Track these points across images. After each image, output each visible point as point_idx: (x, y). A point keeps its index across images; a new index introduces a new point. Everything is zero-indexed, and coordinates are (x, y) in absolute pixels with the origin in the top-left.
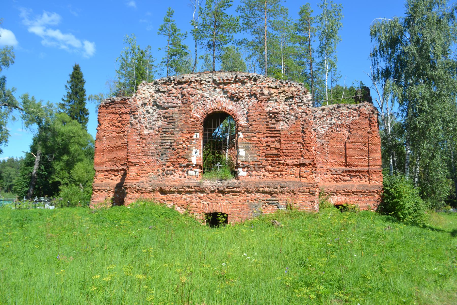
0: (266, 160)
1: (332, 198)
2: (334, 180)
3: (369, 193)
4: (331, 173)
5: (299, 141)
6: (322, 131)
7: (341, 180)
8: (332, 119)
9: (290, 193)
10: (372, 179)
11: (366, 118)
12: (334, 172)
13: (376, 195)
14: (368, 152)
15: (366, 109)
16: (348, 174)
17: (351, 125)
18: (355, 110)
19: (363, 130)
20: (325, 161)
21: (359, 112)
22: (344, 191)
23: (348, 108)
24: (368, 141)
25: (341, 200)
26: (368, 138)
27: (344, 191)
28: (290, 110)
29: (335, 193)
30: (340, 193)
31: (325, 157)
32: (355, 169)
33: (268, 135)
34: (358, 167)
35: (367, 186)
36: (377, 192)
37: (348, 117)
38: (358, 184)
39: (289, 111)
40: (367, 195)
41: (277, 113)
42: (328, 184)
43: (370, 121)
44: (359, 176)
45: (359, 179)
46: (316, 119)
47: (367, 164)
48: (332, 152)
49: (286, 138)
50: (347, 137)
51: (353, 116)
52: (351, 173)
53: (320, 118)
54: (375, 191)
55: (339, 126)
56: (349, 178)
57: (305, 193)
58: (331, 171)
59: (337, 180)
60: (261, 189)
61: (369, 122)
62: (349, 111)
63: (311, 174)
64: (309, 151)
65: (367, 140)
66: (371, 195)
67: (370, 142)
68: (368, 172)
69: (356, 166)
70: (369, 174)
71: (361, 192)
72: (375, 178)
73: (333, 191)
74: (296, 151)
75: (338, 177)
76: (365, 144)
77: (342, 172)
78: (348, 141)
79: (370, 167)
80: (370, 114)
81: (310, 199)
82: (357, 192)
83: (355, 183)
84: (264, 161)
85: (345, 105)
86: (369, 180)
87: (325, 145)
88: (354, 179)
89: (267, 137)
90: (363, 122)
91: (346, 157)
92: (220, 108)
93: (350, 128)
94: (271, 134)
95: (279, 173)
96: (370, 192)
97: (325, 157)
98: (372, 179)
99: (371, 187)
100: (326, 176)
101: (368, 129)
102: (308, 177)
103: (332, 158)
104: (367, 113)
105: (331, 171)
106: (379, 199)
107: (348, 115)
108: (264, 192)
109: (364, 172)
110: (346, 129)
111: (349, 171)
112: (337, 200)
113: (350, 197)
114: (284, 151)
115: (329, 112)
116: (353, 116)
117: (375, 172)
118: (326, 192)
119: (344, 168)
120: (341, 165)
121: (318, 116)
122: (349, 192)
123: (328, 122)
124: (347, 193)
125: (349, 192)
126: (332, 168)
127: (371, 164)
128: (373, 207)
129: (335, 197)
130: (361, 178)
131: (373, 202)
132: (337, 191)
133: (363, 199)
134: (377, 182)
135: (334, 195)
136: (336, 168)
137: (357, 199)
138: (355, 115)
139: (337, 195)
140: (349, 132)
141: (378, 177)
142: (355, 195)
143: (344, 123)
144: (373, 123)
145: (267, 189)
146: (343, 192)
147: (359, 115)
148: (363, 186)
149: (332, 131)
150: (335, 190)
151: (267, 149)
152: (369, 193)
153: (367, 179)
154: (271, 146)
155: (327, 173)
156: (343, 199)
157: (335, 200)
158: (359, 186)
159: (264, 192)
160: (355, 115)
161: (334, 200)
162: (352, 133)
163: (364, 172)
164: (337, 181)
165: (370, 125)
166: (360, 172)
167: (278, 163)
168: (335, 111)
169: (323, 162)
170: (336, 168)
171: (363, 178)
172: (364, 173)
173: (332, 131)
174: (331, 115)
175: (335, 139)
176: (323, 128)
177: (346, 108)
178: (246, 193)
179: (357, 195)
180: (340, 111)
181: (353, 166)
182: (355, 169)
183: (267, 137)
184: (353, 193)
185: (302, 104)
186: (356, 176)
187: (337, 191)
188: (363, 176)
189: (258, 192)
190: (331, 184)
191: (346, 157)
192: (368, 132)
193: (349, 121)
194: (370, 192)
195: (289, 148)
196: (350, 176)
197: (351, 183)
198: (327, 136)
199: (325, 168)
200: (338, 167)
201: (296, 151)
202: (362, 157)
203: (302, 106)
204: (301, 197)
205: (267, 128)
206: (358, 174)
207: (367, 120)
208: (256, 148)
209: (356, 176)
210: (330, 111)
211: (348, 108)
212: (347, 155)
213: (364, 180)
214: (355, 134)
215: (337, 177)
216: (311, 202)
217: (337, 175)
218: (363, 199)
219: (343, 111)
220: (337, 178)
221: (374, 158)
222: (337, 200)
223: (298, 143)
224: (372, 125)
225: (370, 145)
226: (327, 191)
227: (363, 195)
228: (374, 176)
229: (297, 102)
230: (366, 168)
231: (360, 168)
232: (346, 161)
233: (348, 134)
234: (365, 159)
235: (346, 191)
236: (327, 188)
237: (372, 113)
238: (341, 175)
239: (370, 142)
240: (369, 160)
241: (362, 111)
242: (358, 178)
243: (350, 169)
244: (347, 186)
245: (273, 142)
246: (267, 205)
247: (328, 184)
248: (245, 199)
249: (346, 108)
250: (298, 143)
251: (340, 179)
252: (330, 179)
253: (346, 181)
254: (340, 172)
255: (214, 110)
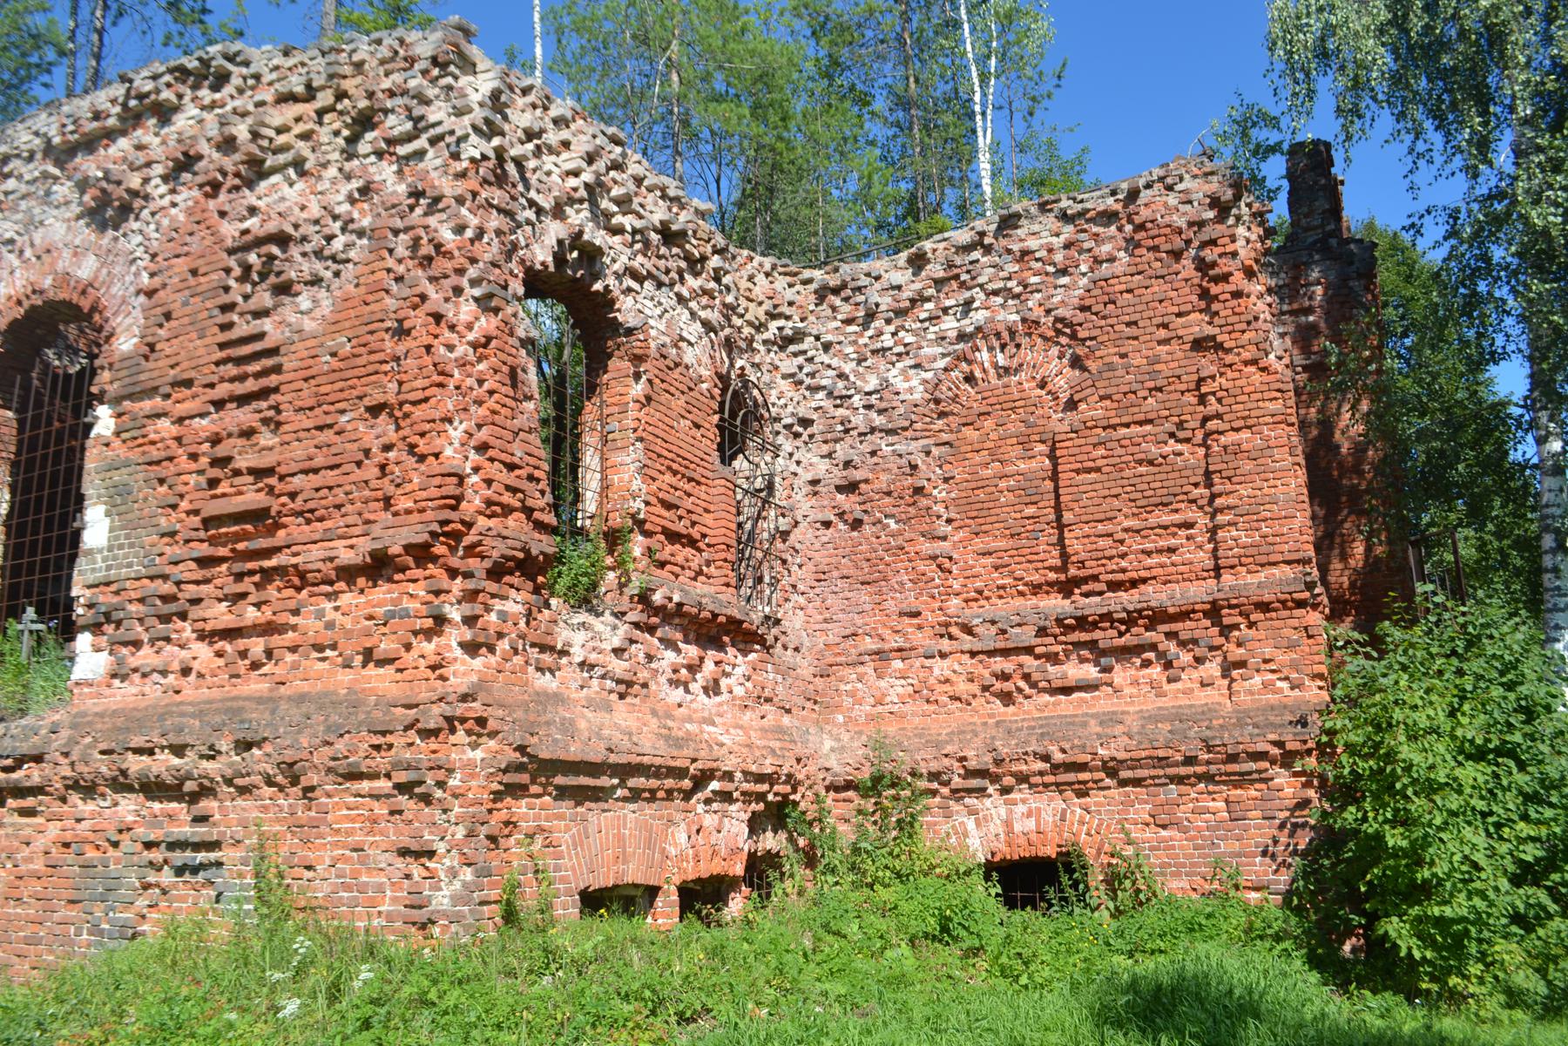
0: (204, 562)
1: (972, 812)
2: (985, 688)
3: (1222, 766)
4: (967, 642)
5: (376, 397)
6: (911, 386)
7: (1034, 685)
8: (968, 305)
9: (281, 789)
10: (1242, 664)
11: (1177, 255)
12: (988, 637)
13: (1281, 777)
14: (1208, 474)
15: (1172, 200)
16: (1078, 645)
17: (1080, 317)
18: (1109, 217)
19: (1163, 333)
20: (930, 569)
21: (1129, 228)
22: (1046, 758)
23: (1065, 217)
24: (1202, 400)
25: (1031, 824)
26: (1200, 381)
27: (1046, 758)
28: (352, 201)
29: (985, 777)
30: (1022, 778)
31: (927, 547)
32: (1128, 599)
33: (223, 390)
34: (1148, 589)
35: (1208, 712)
36: (1287, 759)
37: (1064, 272)
38: (1152, 704)
39: (344, 208)
40: (1208, 778)
41: (282, 240)
42: (946, 721)
43: (1202, 266)
44: (1153, 647)
45: (1156, 671)
46: (878, 323)
47: (1203, 558)
48: (975, 512)
49: (308, 390)
50: (1064, 397)
51: (1098, 261)
52: (1097, 634)
53: (901, 313)
54: (1262, 747)
55: (1007, 339)
56: (1091, 672)
57: (365, 785)
58: (968, 630)
59: (1008, 686)
60: (135, 764)
61: (1196, 277)
62: (1068, 231)
63: (428, 634)
64: (422, 458)
65: (1190, 398)
66: (1242, 780)
67: (1213, 406)
68: (1214, 611)
69: (1134, 583)
70: (1226, 631)
71: (1162, 761)
72: (1268, 652)
73: (972, 764)
74: (359, 475)
75: (1010, 666)
76: (1180, 425)
77: (1042, 632)
78: (1059, 422)
79: (1227, 578)
80: (1201, 224)
81: (396, 834)
82: (1136, 763)
83: (1133, 702)
84: (189, 571)
85: (1043, 207)
86: (1228, 668)
87: (929, 471)
88: (1122, 674)
89: (219, 404)
90: (1158, 287)
91: (1061, 527)
92: (48, 282)
93: (1073, 336)
94: (242, 378)
95: (257, 646)
96: (1233, 758)
97: (927, 547)
98: (1242, 664)
99: (1241, 724)
100: (940, 667)
101: (1197, 325)
102: (409, 658)
103: (979, 544)
104: (1181, 222)
105: (968, 630)
106: (1304, 804)
107: (1059, 257)
108: (153, 789)
109: (1184, 615)
110: (1055, 351)
111: (1082, 623)
112: (1008, 824)
113: (1096, 798)
114: (297, 481)
115: (950, 265)
116: (1098, 261)
117: (1264, 607)
118: (934, 776)
119: (1056, 604)
120: (1036, 589)
121: (886, 302)
122: (1083, 767)
123: (950, 324)
124: (1069, 775)
125: (1083, 767)
126: (975, 614)
127: (1228, 555)
128: (1260, 868)
129: (993, 805)
130: (1168, 665)
131: (1259, 832)
132: (998, 762)
133: (1181, 813)
134: (1282, 678)
135: (981, 792)
136: (1002, 608)
137: (1142, 811)
138: (1106, 248)
139: (1006, 791)
140: (1076, 362)
141: (1291, 647)
142: (1123, 783)
143: (1038, 313)
144: (1225, 278)
145: (163, 764)
146: (1040, 765)
147: (1132, 245)
148: (1178, 716)
149: (970, 379)
150: (988, 758)
151: (213, 483)
152: (1222, 766)
153: (1213, 668)
154: (241, 463)
155: (945, 645)
156: (1048, 818)
157: (996, 827)
158: (1155, 718)
159: (153, 789)
160: (1106, 248)
161: (988, 827)
162: (1092, 365)
163: (1184, 615)
164: (1007, 698)
165: (1204, 294)
166: (1157, 617)
167: (262, 570)
168: (988, 250)
169: (919, 579)
170: (1002, 608)
171: (1186, 657)
172: (1184, 628)
173: (970, 379)
174: (963, 285)
175: (989, 423)
176: (917, 366)
177: (1050, 221)
178: (74, 798)
179: (1137, 782)
180: (1015, 247)
181: (1114, 586)
182: (1128, 599)
183: (219, 404)
184: (1111, 769)
185: (421, 143)
186: (1138, 649)
187: (998, 762)
188: (1183, 644)
189: (121, 783)
190: (967, 716)
191: (1061, 527)
192: (1199, 345)
193: (1066, 296)
194: (1233, 758)
195: (319, 461)
196: (1097, 652)
197: (1101, 702)
198: (942, 415)
199: (929, 617)
200: (1019, 602)
201: (359, 475)
202: (1166, 519)
203: (420, 154)
204: (343, 807)
205: (222, 346)
206: (1117, 631)
207: (1187, 267)
208: (163, 489)
209: (1138, 649)
210: (958, 261)
211: (1065, 217)
212: (1068, 517)
213: (1190, 678)
214: (1111, 367)
215: (1006, 665)
216: (404, 852)
217: (1005, 652)
218: (1181, 813)
219: (1032, 244)
220: (1005, 677)
221: (1252, 515)
222: (1008, 824)
223: (375, 410)
224: (1215, 289)
225: (1212, 425)
226: (934, 766)
227: (1180, 780)
228: (1260, 641)
229: (391, 142)
230: (1199, 592)
231: (1155, 595)
232: (1064, 556)
233: (1064, 380)
234: (1188, 525)
235: (1058, 757)
236: (938, 745)
237: (1211, 214)
238: (1029, 650)
239: (1213, 406)
240: (1213, 531)
241: (1145, 214)
242: (1147, 664)
243: (1091, 606)
244: (1071, 722)
245: (248, 433)
246: (167, 877)
247: (946, 721)
248: (68, 836)
249: (1050, 221)
250: (375, 410)
251: (1026, 677)
252: (963, 687)
253: (1067, 691)
254: (1026, 636)
255: (26, 304)
